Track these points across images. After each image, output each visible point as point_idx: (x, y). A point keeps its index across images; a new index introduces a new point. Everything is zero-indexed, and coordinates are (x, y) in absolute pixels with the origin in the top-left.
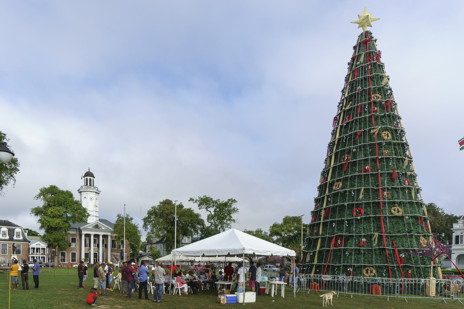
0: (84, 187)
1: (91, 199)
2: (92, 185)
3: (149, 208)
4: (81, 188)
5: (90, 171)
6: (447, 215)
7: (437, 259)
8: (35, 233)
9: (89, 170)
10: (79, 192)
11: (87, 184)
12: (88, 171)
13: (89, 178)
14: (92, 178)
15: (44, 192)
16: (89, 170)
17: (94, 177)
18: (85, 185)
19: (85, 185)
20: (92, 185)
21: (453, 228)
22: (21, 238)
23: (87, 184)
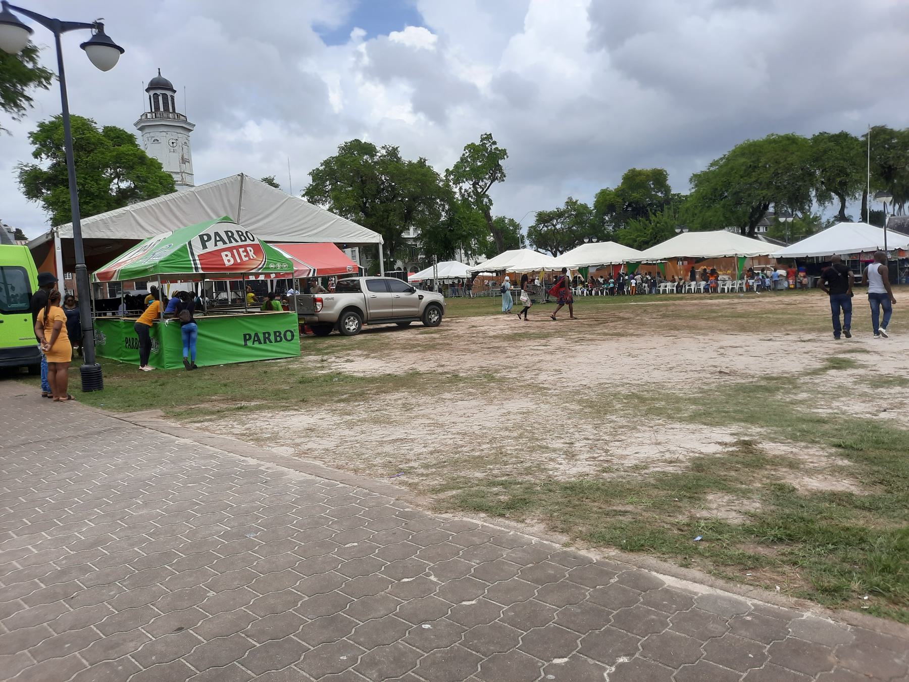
0: (149, 115)
1: (173, 143)
2: (171, 110)
3: (317, 164)
4: (144, 117)
5: (163, 76)
6: (623, 184)
7: (577, 622)
8: (774, 141)
9: (159, 73)
10: (139, 127)
11: (157, 108)
12: (156, 75)
13: (159, 92)
14: (169, 93)
15: (691, 180)
16: (159, 73)
17: (175, 91)
18: (153, 110)
19: (153, 110)
20: (171, 110)
21: (228, 299)
22: (11, 293)
23: (157, 108)
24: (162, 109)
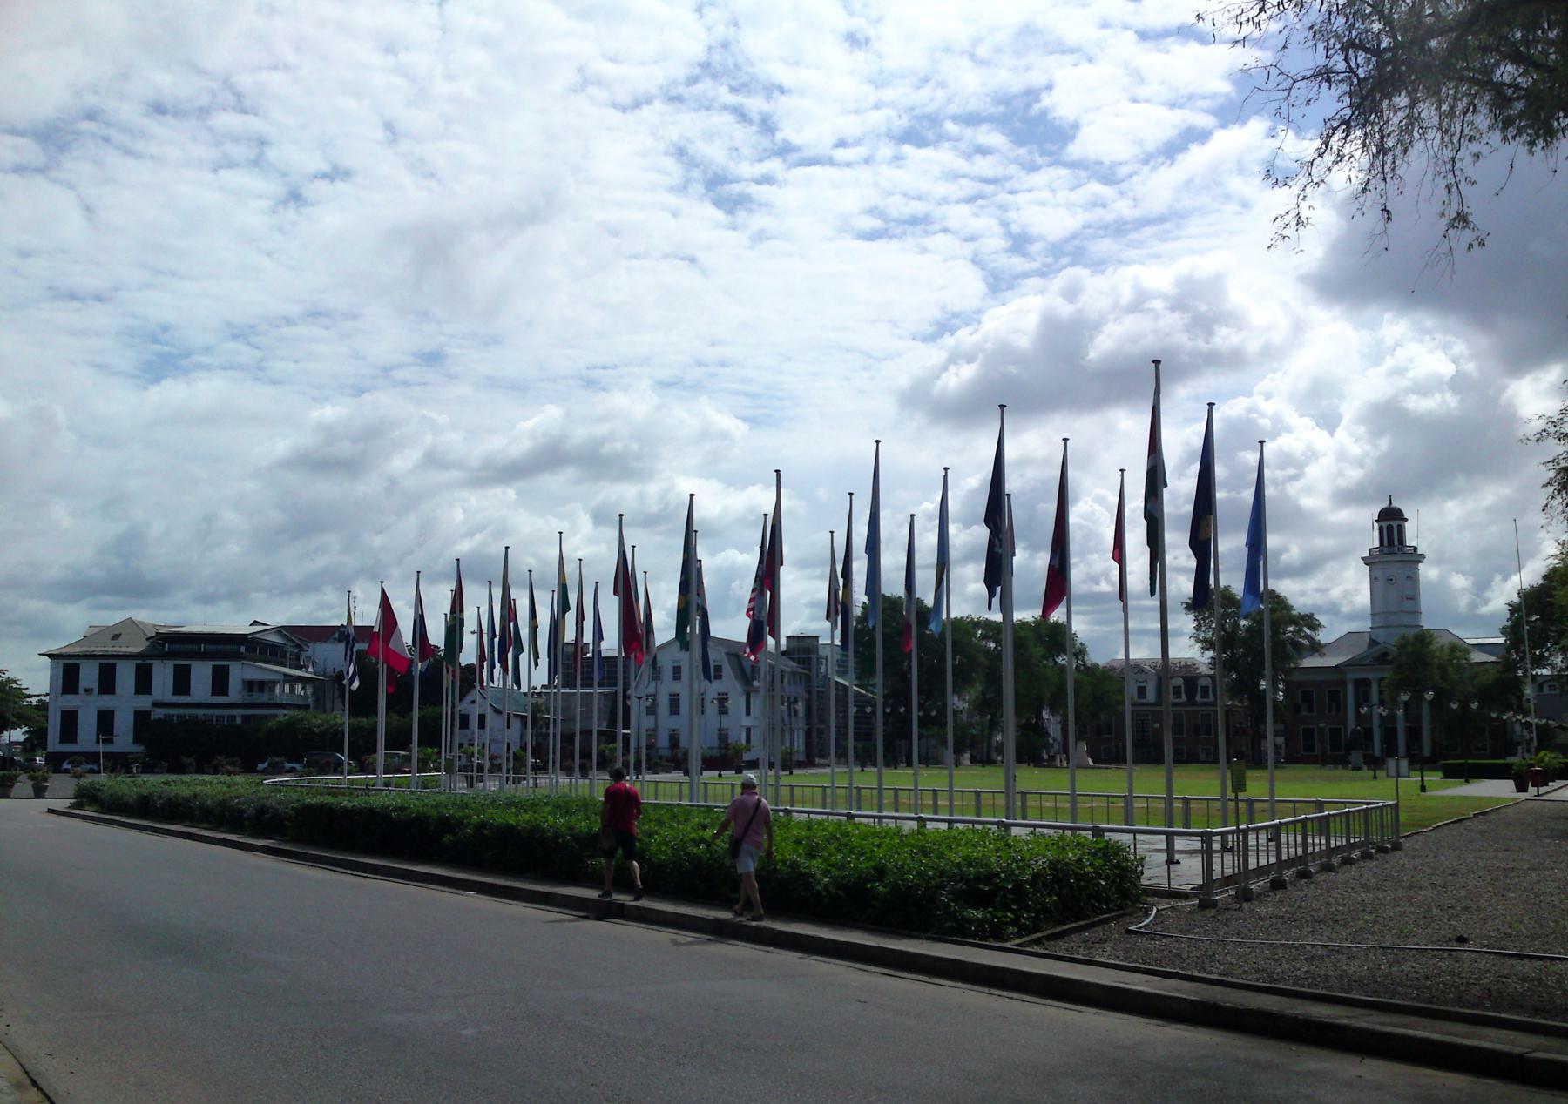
5: (1395, 504)
12: (1385, 505)
13: (1385, 524)
14: (1395, 524)
16: (1390, 500)
24: (1396, 542)
